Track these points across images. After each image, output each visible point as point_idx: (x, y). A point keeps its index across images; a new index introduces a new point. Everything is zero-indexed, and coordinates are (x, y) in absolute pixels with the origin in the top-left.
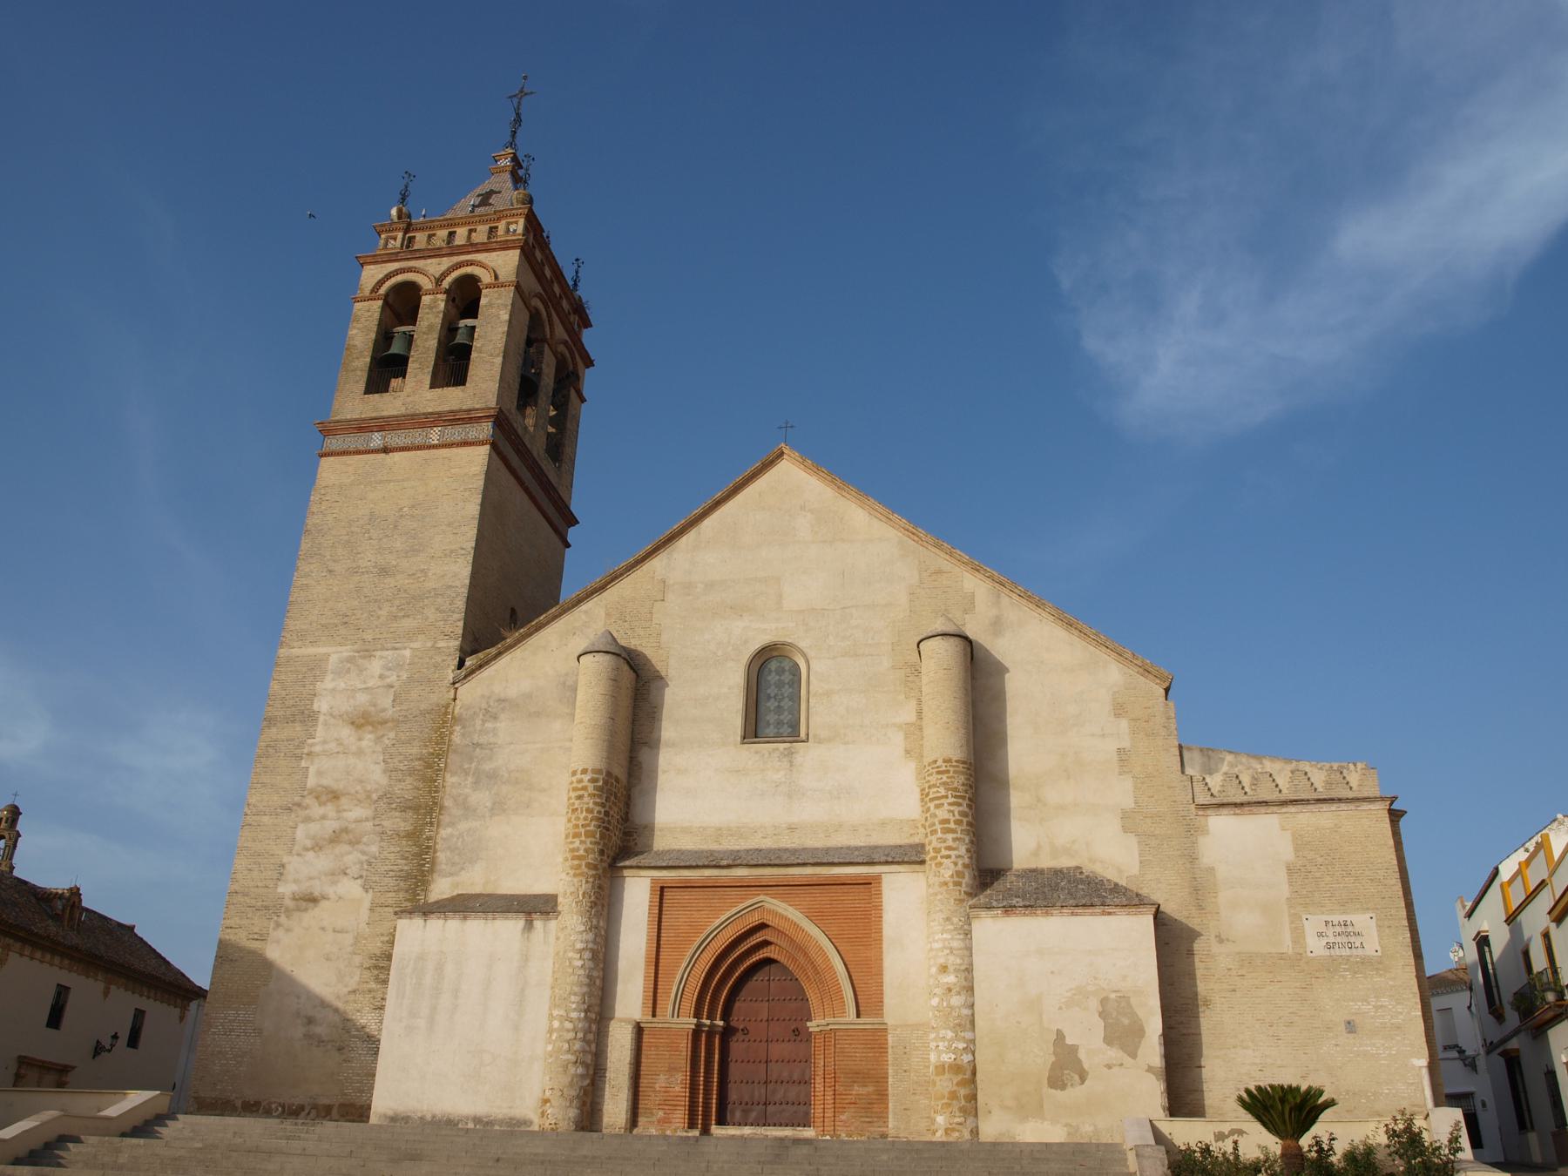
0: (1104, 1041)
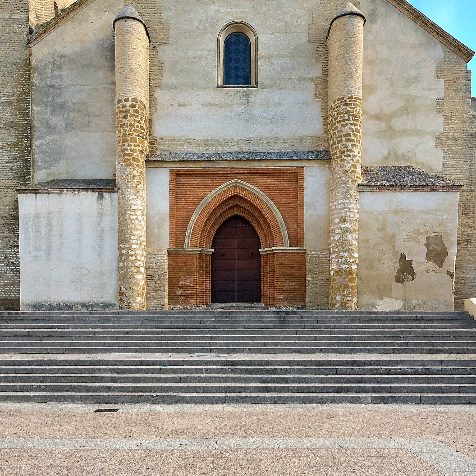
0: (426, 259)
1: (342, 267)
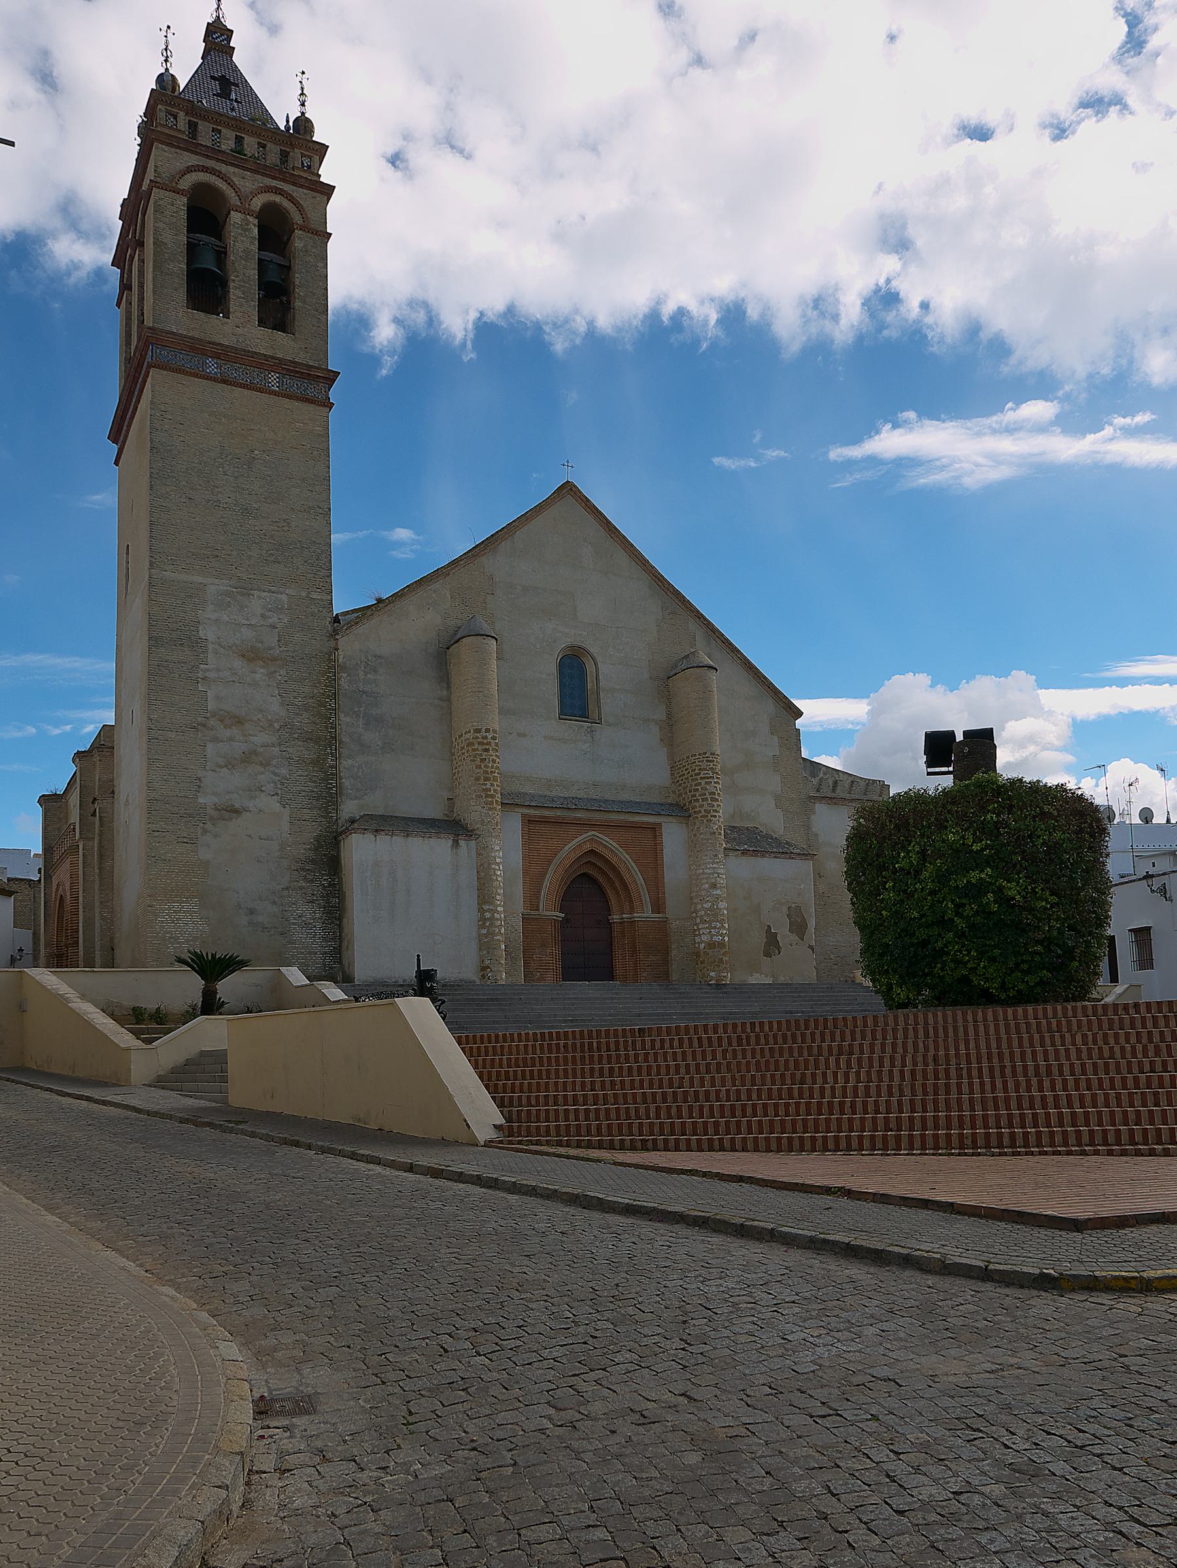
1: (716, 938)
